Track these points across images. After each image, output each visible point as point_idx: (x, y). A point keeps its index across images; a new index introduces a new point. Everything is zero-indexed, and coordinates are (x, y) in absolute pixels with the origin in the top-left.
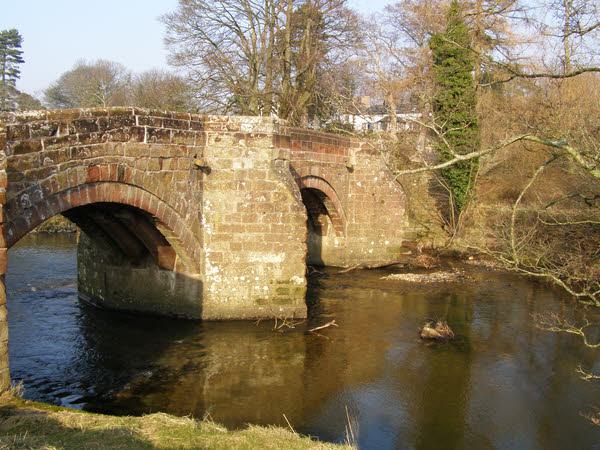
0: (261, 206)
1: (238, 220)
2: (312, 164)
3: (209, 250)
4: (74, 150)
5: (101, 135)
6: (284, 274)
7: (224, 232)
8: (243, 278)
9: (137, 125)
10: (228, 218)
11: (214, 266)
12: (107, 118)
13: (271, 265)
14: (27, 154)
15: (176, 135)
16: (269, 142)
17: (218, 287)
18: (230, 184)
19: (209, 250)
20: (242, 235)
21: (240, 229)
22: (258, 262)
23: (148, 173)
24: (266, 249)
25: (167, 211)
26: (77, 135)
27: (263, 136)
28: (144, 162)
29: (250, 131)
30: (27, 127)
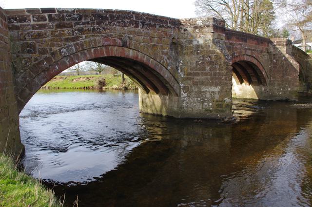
0: (208, 62)
1: (196, 70)
2: (247, 49)
3: (182, 85)
4: (94, 29)
5: (111, 23)
6: (220, 97)
7: (189, 76)
8: (199, 99)
9: (134, 19)
10: (191, 69)
11: (185, 93)
12: (114, 14)
13: (213, 92)
14: (64, 29)
15: (160, 26)
16: (211, 29)
17: (187, 103)
18: (192, 52)
19: (182, 85)
20: (198, 77)
21: (198, 74)
22: (206, 91)
23: (142, 44)
24: (211, 84)
25: (156, 64)
26: (95, 21)
27: (208, 26)
28: (141, 38)
29: (201, 24)
30: (63, 16)
